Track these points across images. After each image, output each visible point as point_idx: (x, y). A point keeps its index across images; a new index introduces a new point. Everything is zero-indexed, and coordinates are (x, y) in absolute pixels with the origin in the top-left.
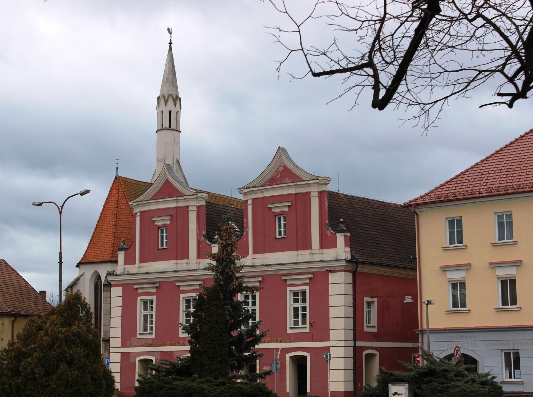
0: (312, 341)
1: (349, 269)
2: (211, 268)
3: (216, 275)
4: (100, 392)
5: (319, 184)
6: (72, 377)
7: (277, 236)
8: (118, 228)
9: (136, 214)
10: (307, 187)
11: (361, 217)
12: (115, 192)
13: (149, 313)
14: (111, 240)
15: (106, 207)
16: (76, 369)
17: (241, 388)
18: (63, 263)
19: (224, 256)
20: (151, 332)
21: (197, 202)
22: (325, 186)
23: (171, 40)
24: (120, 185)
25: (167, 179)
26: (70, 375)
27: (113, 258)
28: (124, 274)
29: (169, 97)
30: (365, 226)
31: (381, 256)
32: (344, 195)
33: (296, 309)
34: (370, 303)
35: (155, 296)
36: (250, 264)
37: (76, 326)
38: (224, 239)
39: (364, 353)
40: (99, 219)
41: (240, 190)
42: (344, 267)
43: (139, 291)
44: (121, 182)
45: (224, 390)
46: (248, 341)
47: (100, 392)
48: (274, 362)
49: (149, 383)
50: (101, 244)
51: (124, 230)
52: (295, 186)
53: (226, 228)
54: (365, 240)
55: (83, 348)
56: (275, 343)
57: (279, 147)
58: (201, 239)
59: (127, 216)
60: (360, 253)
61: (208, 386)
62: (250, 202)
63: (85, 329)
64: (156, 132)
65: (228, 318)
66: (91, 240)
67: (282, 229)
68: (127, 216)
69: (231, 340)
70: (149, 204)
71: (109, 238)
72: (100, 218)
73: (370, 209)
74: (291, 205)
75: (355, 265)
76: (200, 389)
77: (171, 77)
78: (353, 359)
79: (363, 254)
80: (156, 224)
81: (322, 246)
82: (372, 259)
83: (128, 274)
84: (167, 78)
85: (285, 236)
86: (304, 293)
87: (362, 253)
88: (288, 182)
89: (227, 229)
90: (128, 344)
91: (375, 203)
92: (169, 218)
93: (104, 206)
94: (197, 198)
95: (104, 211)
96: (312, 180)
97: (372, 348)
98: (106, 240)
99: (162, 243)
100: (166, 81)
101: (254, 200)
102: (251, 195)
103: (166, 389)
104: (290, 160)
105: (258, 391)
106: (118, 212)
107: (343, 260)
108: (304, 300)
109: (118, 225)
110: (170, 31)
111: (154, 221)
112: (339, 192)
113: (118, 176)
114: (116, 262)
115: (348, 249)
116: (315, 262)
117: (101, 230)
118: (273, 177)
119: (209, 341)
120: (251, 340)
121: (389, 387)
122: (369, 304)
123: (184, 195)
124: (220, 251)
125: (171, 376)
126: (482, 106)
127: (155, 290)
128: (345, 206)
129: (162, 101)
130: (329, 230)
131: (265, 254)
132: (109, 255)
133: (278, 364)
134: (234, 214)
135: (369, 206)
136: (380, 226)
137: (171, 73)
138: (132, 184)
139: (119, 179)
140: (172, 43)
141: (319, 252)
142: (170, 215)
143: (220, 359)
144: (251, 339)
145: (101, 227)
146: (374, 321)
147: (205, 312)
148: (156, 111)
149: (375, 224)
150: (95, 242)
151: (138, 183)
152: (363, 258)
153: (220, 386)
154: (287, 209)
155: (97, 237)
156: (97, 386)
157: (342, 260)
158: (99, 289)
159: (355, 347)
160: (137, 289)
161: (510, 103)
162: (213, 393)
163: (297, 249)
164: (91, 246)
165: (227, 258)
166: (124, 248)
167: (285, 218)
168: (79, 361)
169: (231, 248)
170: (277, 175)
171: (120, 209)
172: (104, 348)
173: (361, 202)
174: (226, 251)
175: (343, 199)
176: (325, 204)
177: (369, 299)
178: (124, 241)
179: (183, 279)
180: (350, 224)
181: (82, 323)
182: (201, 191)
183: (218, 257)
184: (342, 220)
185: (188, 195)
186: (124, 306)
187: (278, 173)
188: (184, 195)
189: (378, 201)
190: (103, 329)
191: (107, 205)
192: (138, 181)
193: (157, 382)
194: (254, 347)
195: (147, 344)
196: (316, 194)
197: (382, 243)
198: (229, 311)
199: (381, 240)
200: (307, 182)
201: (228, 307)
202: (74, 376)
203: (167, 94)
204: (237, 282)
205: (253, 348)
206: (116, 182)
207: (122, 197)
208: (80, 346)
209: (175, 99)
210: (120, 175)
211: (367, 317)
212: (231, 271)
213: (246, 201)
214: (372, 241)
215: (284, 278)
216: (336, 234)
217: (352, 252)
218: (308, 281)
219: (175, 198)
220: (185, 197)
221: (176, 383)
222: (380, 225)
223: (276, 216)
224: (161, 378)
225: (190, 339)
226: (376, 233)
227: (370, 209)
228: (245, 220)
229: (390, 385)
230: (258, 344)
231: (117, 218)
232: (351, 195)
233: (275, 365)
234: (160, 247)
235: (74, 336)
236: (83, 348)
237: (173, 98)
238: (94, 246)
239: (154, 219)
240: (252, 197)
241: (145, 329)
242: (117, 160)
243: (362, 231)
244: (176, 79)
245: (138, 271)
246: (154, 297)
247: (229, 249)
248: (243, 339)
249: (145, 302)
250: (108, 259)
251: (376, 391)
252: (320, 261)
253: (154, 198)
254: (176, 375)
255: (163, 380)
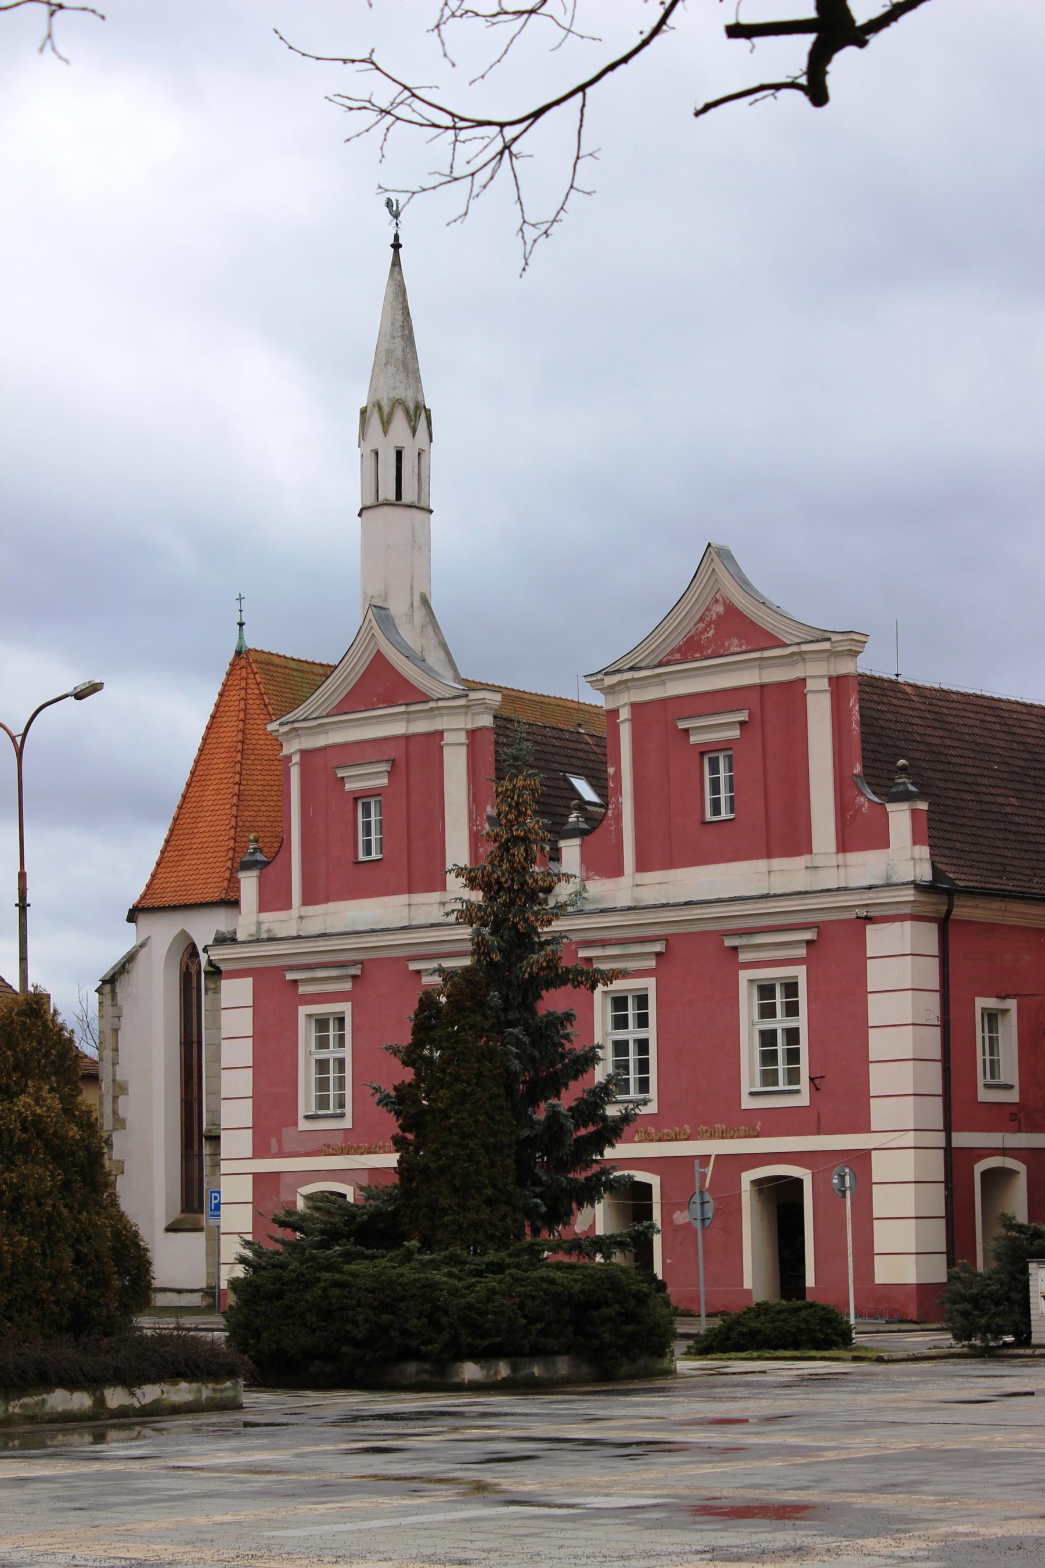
0: (819, 1133)
1: (928, 910)
2: (468, 915)
3: (478, 933)
4: (102, 1301)
5: (833, 655)
6: (14, 1254)
7: (709, 817)
8: (246, 803)
9: (289, 758)
10: (795, 663)
11: (967, 753)
12: (234, 695)
13: (331, 1053)
14: (227, 838)
15: (208, 741)
16: (29, 1229)
17: (552, 1281)
18: (29, 905)
19: (503, 875)
20: (339, 1111)
21: (469, 717)
22: (849, 658)
23: (397, 237)
24: (252, 676)
25: (378, 652)
26: (6, 1248)
27: (232, 894)
28: (258, 941)
29: (393, 407)
30: (980, 780)
31: (1029, 872)
32: (915, 687)
33: (768, 1037)
34: (996, 1015)
35: (349, 1005)
36: (627, 903)
37: (31, 1095)
38: (504, 821)
39: (980, 1167)
40: (191, 778)
41: (595, 678)
42: (910, 905)
43: (302, 989)
44: (253, 665)
45: (497, 1286)
46: (582, 1137)
47: (102, 1301)
48: (697, 1198)
49: (274, 1266)
50: (196, 851)
51: (263, 809)
52: (757, 663)
53: (510, 787)
54: (978, 823)
55: (50, 1166)
56: (708, 1138)
57: (709, 545)
58: (483, 828)
59: (273, 768)
60: (962, 863)
61: (451, 1275)
62: (625, 714)
63: (57, 1105)
64: (360, 515)
65: (516, 1065)
66: (167, 841)
67: (723, 795)
68: (273, 768)
69: (526, 1133)
70: (327, 727)
71: (219, 834)
72: (193, 773)
73: (997, 727)
74: (747, 719)
75: (945, 898)
76: (423, 1287)
77: (400, 348)
78: (943, 1185)
79: (972, 867)
80: (349, 786)
81: (844, 845)
82: (1001, 881)
83: (270, 940)
84: (387, 350)
85: (732, 816)
86: (791, 988)
87: (968, 863)
88: (738, 649)
89: (513, 791)
90: (274, 1148)
91: (1012, 711)
92: (385, 767)
93: (205, 739)
94: (467, 707)
95: (206, 752)
96: (812, 642)
97: (1003, 1152)
98: (211, 839)
99: (368, 844)
100: (384, 361)
101: (635, 706)
102: (626, 694)
103: (323, 1285)
104: (743, 583)
105: (608, 1289)
106: (245, 756)
107: (907, 883)
108: (792, 1010)
109: (246, 793)
110: (394, 208)
111: (343, 778)
112: (901, 680)
113: (244, 649)
114: (234, 904)
115: (924, 851)
116: (822, 891)
117: (195, 810)
118: (692, 637)
119: (455, 1137)
120: (592, 1133)
121: (1030, 1271)
122: (992, 1017)
123: (427, 699)
124: (492, 860)
125: (340, 1246)
126: (707, 107)
127: (347, 986)
128: (917, 721)
129: (375, 422)
130: (862, 794)
131: (672, 872)
132: (220, 885)
133: (706, 1205)
134: (536, 743)
135: (994, 719)
136: (1029, 780)
137: (400, 334)
138: (287, 671)
139: (247, 659)
140: (400, 246)
141: (835, 859)
142: (387, 761)
143: (489, 1191)
144: (591, 1129)
145: (198, 799)
146: (1010, 1071)
147: (441, 1048)
148: (358, 452)
149: (1013, 772)
150: (180, 848)
151: (307, 668)
152: (971, 878)
153: (486, 1277)
154: (735, 733)
155: (186, 831)
156: (90, 1278)
157: (903, 884)
158: (194, 984)
159: (949, 1151)
160: (295, 982)
161: (809, 80)
162: (463, 1296)
163: (769, 855)
164: (166, 860)
165: (513, 881)
166: (257, 861)
167: (730, 758)
168: (40, 1204)
169: (526, 851)
170: (705, 630)
171: (251, 747)
172: (211, 1160)
173: (969, 708)
174: (509, 861)
175: (914, 698)
176: (850, 715)
177: (992, 1003)
178: (256, 841)
179: (429, 952)
180: (931, 774)
181: (47, 1087)
182: (481, 683)
183: (486, 879)
184: (902, 762)
185: (440, 699)
186: (261, 1036)
187: (709, 625)
188: (427, 699)
189: (1024, 705)
190: (207, 1105)
191: (213, 736)
192: (306, 662)
193: (295, 1265)
194: (602, 1155)
195: (329, 1147)
196: (824, 684)
197: (1032, 830)
198: (518, 1043)
199: (1030, 821)
200: (795, 649)
201: (516, 1031)
202: (21, 1250)
203: (388, 398)
204: (543, 953)
205: (599, 1157)
206: (237, 668)
207: (258, 711)
208: (44, 1159)
209: (411, 412)
210: (250, 644)
211: (988, 1057)
212: (526, 920)
213: (614, 713)
214: (1002, 826)
215: (729, 942)
216: (887, 805)
217: (938, 859)
218: (802, 952)
219: (402, 709)
220: (432, 704)
221: (352, 1267)
222: (1029, 776)
223: (702, 754)
224: (307, 1252)
225: (399, 1131)
226: (1013, 801)
227: (997, 727)
228: (611, 770)
229: (1032, 1267)
230: (612, 1145)
231: (244, 772)
232: (937, 686)
233: (698, 1206)
234: (362, 857)
235: (24, 1130)
236: (50, 1166)
237: (407, 411)
238: (177, 859)
239: (341, 774)
240: (629, 698)
241: (323, 1102)
242: (240, 599)
243: (969, 797)
244: (415, 353)
245: (299, 930)
246: (346, 1008)
247: (519, 851)
248: (562, 1130)
249: (322, 1023)
250: (216, 896)
251: (989, 1285)
252: (838, 889)
253: (340, 709)
254: (356, 1244)
255: (313, 1258)
